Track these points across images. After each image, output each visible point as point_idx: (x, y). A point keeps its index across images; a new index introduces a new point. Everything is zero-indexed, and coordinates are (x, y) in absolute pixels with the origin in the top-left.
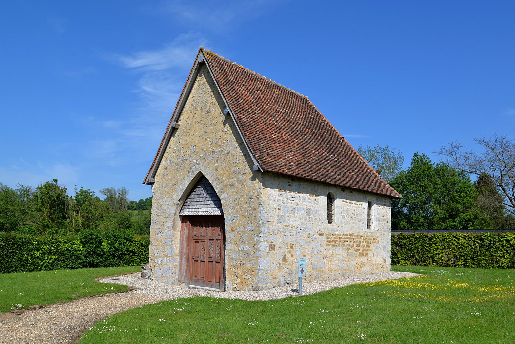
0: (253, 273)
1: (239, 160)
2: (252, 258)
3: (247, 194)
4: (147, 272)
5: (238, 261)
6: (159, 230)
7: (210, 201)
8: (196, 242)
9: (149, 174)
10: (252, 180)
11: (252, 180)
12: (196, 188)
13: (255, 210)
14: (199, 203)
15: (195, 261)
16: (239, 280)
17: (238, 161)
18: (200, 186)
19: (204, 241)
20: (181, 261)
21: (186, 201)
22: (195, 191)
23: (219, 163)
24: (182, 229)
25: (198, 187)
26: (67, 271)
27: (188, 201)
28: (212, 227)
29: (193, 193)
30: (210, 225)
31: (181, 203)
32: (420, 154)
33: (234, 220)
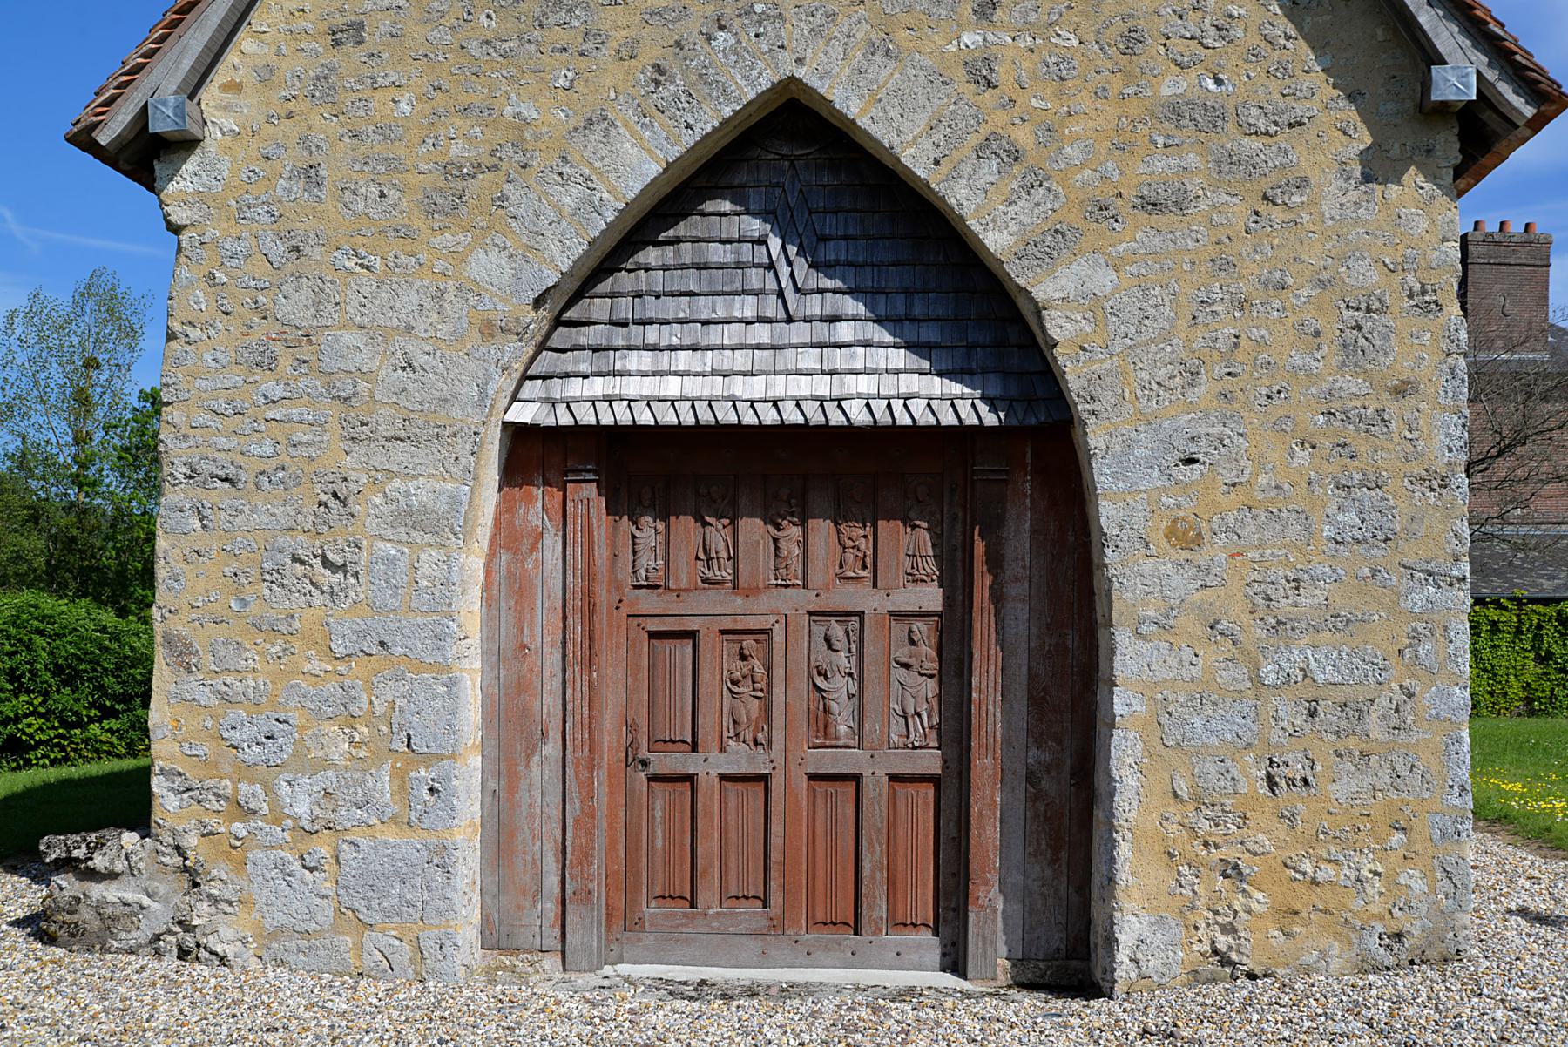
0: (1398, 837)
1: (1222, 22)
2: (1384, 738)
3: (1325, 276)
4: (129, 896)
5: (1250, 759)
6: (285, 541)
7: (855, 319)
8: (653, 635)
9: (150, 55)
10: (1367, 178)
11: (1367, 178)
12: (684, 216)
13: (1401, 390)
14: (731, 334)
15: (653, 779)
16: (1258, 895)
17: (1212, 32)
18: (727, 206)
19: (753, 623)
20: (512, 789)
21: (570, 314)
22: (677, 241)
23: (1004, 28)
24: (507, 537)
25: (708, 206)
26: (771, 970)
27: (595, 317)
28: (839, 517)
29: (651, 255)
30: (744, 501)
31: (538, 321)
32: (1538, 229)
33: (1190, 461)
